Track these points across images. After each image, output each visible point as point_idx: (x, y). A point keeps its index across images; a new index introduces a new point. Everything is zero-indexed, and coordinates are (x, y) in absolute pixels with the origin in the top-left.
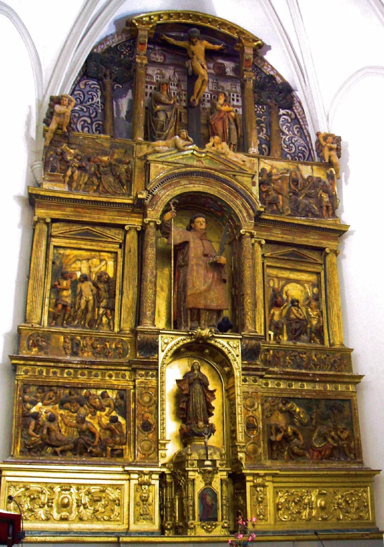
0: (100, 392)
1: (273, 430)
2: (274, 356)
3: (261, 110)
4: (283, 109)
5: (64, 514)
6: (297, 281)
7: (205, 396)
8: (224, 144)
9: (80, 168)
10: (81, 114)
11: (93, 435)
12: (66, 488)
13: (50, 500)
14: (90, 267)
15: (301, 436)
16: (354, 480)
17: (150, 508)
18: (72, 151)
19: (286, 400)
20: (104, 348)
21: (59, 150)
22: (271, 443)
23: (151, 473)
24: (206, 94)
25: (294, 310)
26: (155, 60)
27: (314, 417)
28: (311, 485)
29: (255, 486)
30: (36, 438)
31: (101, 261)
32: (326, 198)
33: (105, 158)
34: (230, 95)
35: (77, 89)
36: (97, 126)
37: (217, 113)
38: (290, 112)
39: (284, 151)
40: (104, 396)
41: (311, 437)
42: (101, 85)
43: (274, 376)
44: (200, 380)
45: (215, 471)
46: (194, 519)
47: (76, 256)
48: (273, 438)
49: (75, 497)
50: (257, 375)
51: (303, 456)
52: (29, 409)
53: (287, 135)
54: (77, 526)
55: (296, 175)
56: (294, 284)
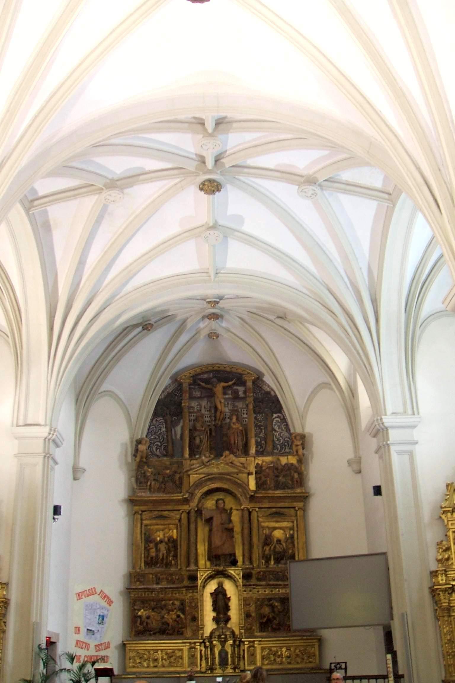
0: (171, 602)
2: (263, 575)
4: (275, 414)
5: (156, 664)
6: (280, 528)
8: (232, 456)
9: (154, 480)
10: (155, 440)
11: (168, 624)
12: (156, 651)
13: (149, 657)
14: (164, 534)
16: (307, 641)
18: (150, 470)
19: (270, 600)
20: (172, 579)
21: (143, 472)
23: (195, 643)
25: (277, 546)
26: (195, 396)
30: (141, 628)
31: (170, 530)
32: (296, 476)
33: (168, 471)
38: (280, 415)
40: (173, 604)
44: (221, 592)
45: (226, 640)
47: (156, 529)
49: (160, 656)
53: (277, 432)
55: (277, 464)
56: (279, 530)
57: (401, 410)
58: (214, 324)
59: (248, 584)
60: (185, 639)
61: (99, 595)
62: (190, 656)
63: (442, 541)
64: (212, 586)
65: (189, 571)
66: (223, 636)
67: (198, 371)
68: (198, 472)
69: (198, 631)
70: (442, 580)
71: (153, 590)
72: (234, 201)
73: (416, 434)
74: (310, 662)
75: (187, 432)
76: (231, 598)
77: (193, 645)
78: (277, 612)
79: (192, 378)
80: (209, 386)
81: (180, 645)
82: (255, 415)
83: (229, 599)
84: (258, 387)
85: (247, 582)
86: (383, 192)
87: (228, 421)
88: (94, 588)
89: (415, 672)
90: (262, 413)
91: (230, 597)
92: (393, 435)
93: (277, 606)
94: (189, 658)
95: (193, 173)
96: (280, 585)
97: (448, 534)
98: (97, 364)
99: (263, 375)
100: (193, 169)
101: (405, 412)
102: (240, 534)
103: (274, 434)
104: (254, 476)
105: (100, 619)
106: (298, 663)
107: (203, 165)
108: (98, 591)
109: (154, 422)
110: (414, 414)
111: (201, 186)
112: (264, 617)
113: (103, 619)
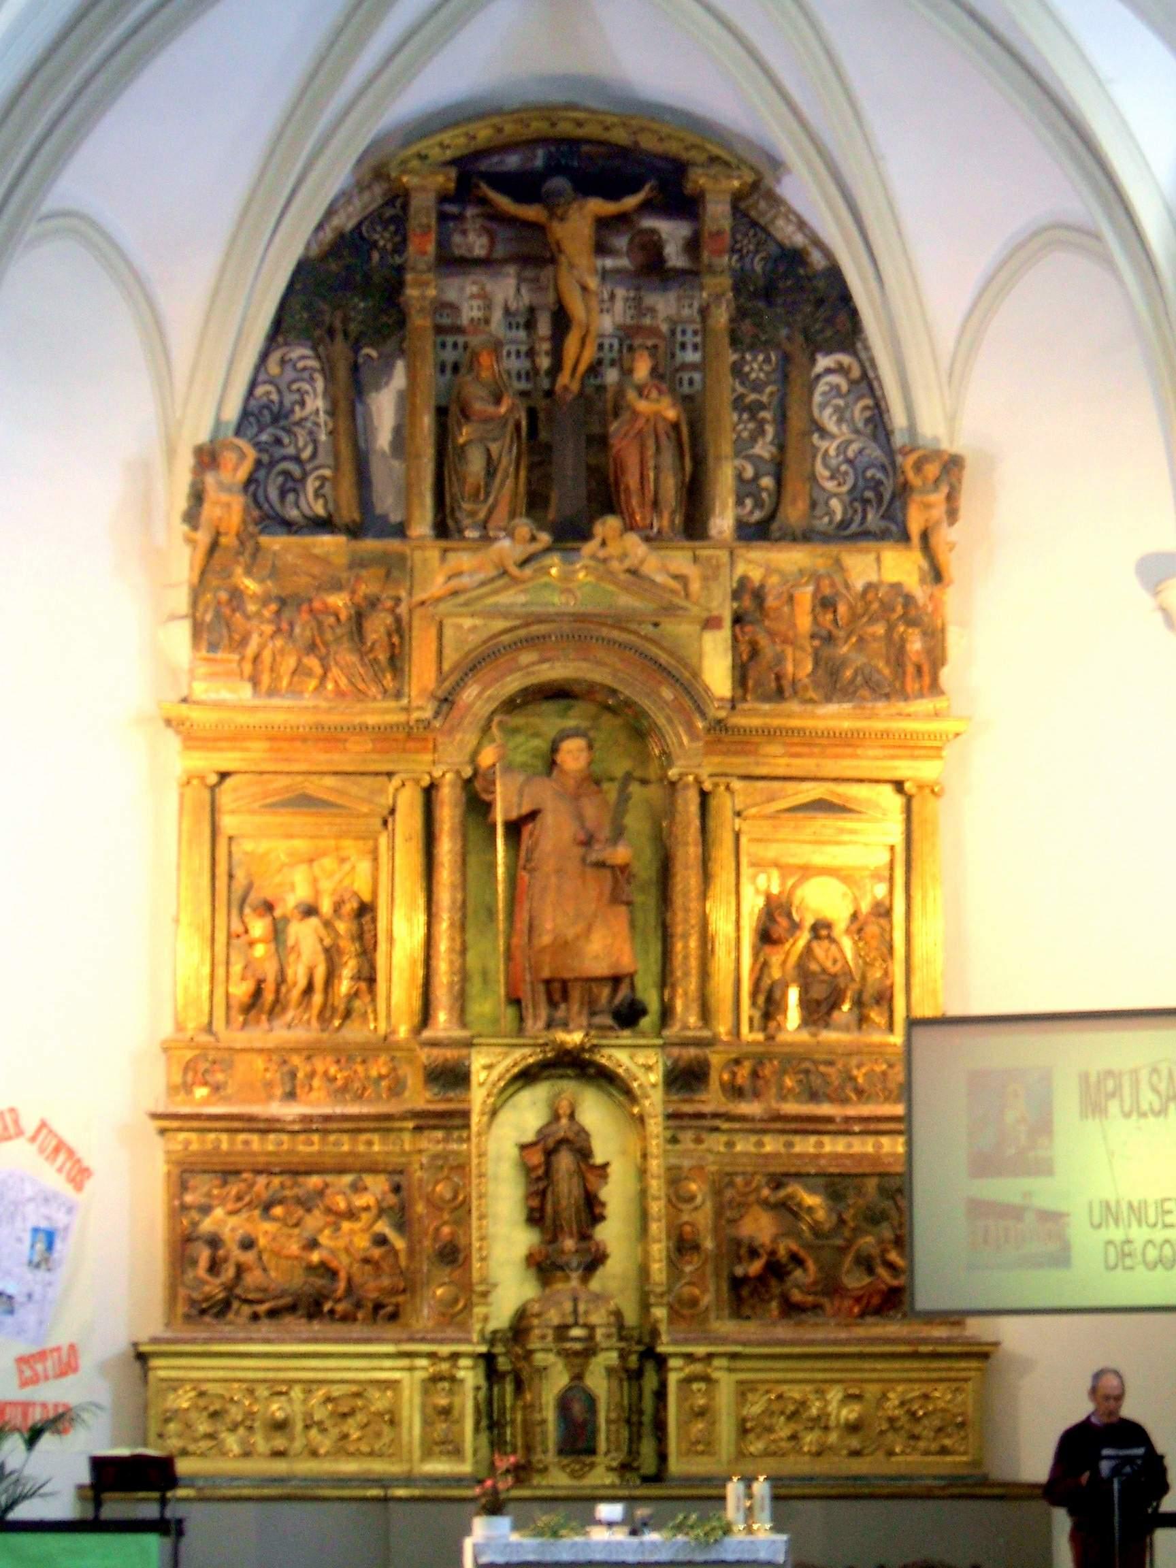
1: (743, 1251)
3: (761, 369)
4: (829, 352)
5: (280, 1443)
7: (584, 1179)
15: (810, 1264)
17: (456, 1428)
19: (777, 1182)
22: (737, 1284)
23: (455, 1356)
24: (607, 342)
25: (819, 949)
27: (847, 1216)
28: (828, 1376)
30: (214, 1288)
32: (915, 645)
34: (673, 332)
35: (262, 377)
36: (317, 484)
37: (626, 416)
38: (845, 359)
39: (823, 489)
41: (837, 1265)
42: (323, 355)
43: (747, 1126)
45: (589, 1351)
46: (545, 1452)
48: (739, 1271)
50: (703, 1128)
51: (816, 1307)
52: (195, 1224)
55: (833, 585)
59: (687, 1108)
60: (411, 1340)
61: (33, 1139)
62: (429, 1411)
64: (527, 1115)
65: (434, 1044)
66: (576, 1332)
67: (484, 134)
68: (478, 607)
69: (468, 1306)
71: (268, 1126)
74: (944, 1451)
75: (427, 421)
76: (610, 1170)
77: (444, 1366)
79: (453, 173)
80: (532, 212)
81: (388, 1363)
82: (734, 357)
83: (602, 1171)
84: (754, 224)
87: (611, 376)
88: (12, 1110)
91: (605, 1166)
93: (810, 1210)
94: (427, 1423)
96: (829, 1119)
98: (36, 86)
99: (777, 164)
102: (654, 891)
103: (815, 449)
104: (725, 633)
105: (40, 1246)
106: (314, 1454)
108: (30, 1126)
109: (273, 367)
112: (753, 1253)
113: (50, 1246)
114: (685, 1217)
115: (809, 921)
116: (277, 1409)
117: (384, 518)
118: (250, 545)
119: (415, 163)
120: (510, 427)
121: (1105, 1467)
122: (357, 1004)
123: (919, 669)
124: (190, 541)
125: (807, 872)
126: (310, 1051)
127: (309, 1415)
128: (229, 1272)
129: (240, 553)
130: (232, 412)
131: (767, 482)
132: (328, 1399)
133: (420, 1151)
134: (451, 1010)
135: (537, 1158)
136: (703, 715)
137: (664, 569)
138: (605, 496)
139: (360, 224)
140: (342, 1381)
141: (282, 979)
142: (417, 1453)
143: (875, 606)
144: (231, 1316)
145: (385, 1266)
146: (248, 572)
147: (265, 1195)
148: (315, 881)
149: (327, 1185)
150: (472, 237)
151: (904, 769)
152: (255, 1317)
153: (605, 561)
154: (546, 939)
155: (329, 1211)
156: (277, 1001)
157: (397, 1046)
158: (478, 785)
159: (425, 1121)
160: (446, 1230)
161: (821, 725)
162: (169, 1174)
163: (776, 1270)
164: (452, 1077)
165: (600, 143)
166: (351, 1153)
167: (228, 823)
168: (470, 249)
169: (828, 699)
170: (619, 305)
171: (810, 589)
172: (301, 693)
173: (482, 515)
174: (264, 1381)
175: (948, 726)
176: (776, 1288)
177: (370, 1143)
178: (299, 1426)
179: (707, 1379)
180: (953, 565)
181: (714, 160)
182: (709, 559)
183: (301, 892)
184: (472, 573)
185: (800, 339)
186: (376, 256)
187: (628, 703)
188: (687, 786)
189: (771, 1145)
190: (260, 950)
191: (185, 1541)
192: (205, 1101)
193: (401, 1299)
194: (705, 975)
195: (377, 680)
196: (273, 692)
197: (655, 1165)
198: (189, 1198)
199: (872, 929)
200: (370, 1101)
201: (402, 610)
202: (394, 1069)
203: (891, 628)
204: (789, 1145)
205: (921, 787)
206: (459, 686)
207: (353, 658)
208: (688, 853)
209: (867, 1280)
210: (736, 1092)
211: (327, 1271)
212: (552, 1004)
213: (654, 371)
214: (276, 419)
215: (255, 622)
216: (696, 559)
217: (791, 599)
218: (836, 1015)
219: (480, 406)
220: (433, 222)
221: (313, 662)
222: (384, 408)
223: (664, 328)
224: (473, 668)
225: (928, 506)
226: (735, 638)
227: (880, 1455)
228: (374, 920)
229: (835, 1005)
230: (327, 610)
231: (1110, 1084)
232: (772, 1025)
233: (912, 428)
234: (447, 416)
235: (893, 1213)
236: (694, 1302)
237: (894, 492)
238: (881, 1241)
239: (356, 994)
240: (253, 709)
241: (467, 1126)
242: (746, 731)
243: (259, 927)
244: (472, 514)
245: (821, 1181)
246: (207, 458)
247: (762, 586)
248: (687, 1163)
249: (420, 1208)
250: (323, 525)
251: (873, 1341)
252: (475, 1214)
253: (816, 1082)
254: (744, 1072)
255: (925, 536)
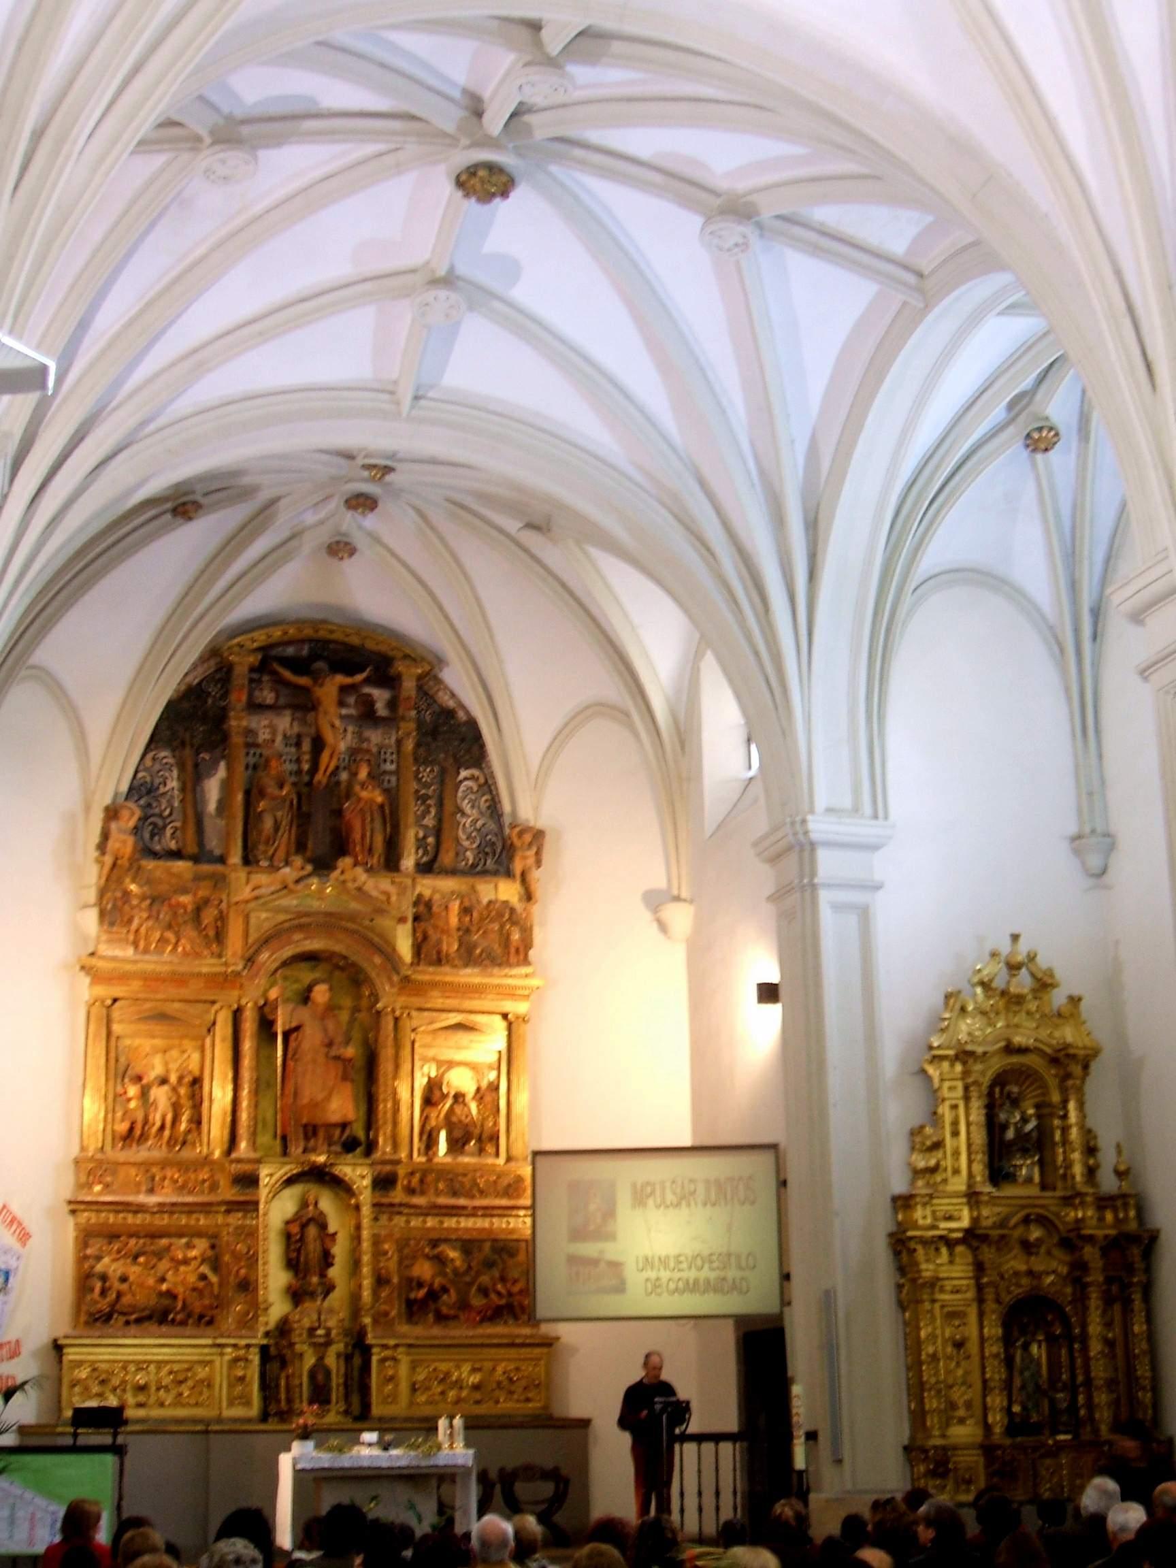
1: (414, 1284)
8: (359, 870)
12: (141, 1366)
13: (124, 1382)
15: (452, 1291)
19: (434, 1243)
22: (410, 1303)
23: (248, 1346)
29: (383, 1361)
30: (104, 1305)
32: (516, 936)
35: (141, 767)
37: (353, 799)
38: (476, 772)
45: (328, 1343)
46: (301, 1402)
48: (412, 1296)
49: (152, 1377)
51: (455, 1317)
52: (92, 1267)
54: (156, 1413)
57: (847, 802)
58: (350, 522)
59: (385, 1200)
60: (222, 1336)
63: (922, 1127)
65: (239, 1161)
67: (277, 633)
68: (271, 905)
69: (256, 1317)
70: (924, 1218)
71: (139, 1209)
72: (516, 222)
73: (882, 866)
74: (528, 1400)
75: (240, 797)
77: (242, 1352)
78: (451, 1275)
84: (426, 694)
85: (382, 1196)
86: (906, 268)
87: (344, 776)
89: (846, 1430)
90: (432, 763)
91: (335, 1234)
92: (828, 864)
95: (445, 135)
96: (464, 1208)
97: (940, 1110)
99: (441, 661)
100: (449, 127)
101: (856, 809)
106: (162, 1405)
107: (474, 120)
109: (148, 762)
110: (876, 817)
111: (463, 178)
113: (7, 1280)
114: (382, 1265)
115: (452, 1093)
116: (141, 1378)
117: (211, 852)
118: (135, 866)
119: (236, 649)
120: (288, 803)
121: (658, 1407)
122: (190, 1137)
123: (517, 951)
124: (99, 862)
125: (451, 1064)
126: (164, 1164)
127: (159, 1381)
128: (112, 1296)
129: (129, 870)
130: (124, 788)
131: (431, 840)
132: (171, 1373)
133: (228, 1225)
134: (248, 1142)
135: (295, 1229)
136: (398, 973)
137: (376, 887)
138: (340, 846)
139: (202, 681)
140: (179, 1362)
141: (146, 1121)
142: (224, 1404)
143: (493, 913)
144: (112, 1322)
145: (206, 1293)
146: (133, 881)
147: (135, 1250)
148: (166, 1064)
149: (171, 1245)
150: (265, 693)
151: (510, 1006)
152: (127, 1323)
153: (344, 882)
154: (305, 1101)
155: (172, 1259)
156: (142, 1135)
157: (213, 1163)
158: (267, 1009)
159: (232, 1207)
160: (243, 1271)
161: (463, 980)
162: (77, 1237)
163: (433, 1295)
164: (249, 1181)
165: (344, 644)
166: (186, 1226)
167: (117, 1028)
168: (265, 699)
169: (466, 965)
170: (349, 736)
171: (457, 903)
172: (163, 952)
173: (270, 853)
174: (133, 1362)
175: (535, 982)
176: (432, 1306)
177: (198, 1220)
178: (153, 1388)
179: (394, 1359)
180: (538, 891)
181: (406, 657)
182: (401, 883)
183: (157, 1070)
184: (268, 886)
185: (451, 760)
186: (210, 701)
187: (354, 965)
188: (387, 1014)
189: (431, 1222)
190: (133, 1104)
191: (128, 1459)
192: (100, 1193)
193: (215, 1312)
194: (395, 1123)
195: (208, 946)
196: (146, 951)
197: (365, 1234)
198: (89, 1251)
199: (488, 1099)
200: (197, 1194)
201: (224, 906)
202: (212, 1176)
203: (502, 926)
204: (441, 1222)
205: (517, 1018)
206: (257, 952)
207: (194, 934)
208: (386, 1053)
209: (484, 1301)
210: (411, 1191)
211: (171, 1295)
212: (307, 1138)
213: (369, 774)
214: (149, 792)
215: (136, 911)
216: (393, 883)
217: (447, 907)
218: (467, 1147)
219: (272, 789)
220: (246, 682)
221: (170, 935)
222: (212, 789)
223: (374, 750)
224: (266, 941)
225: (525, 858)
226: (414, 930)
227: (491, 1403)
228: (201, 1087)
229: (467, 1142)
230: (179, 905)
231: (649, 1189)
232: (431, 1153)
233: (514, 813)
234: (252, 795)
235: (499, 1261)
236: (386, 1314)
237: (506, 849)
238: (492, 1278)
239: (189, 1131)
240: (135, 962)
241: (257, 1210)
242: (422, 983)
243: (133, 1091)
244: (265, 852)
245: (459, 1244)
246: (112, 813)
247: (430, 900)
248: (383, 1233)
249: (227, 1258)
250: (177, 855)
251: (489, 1336)
252: (260, 1262)
253: (457, 1186)
254: (415, 1180)
255: (523, 874)
